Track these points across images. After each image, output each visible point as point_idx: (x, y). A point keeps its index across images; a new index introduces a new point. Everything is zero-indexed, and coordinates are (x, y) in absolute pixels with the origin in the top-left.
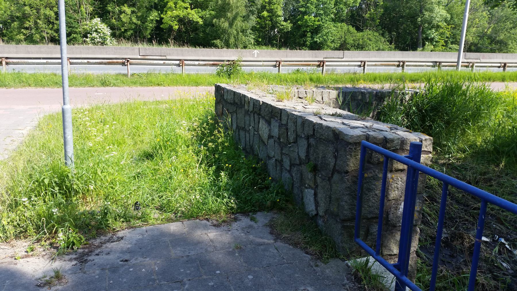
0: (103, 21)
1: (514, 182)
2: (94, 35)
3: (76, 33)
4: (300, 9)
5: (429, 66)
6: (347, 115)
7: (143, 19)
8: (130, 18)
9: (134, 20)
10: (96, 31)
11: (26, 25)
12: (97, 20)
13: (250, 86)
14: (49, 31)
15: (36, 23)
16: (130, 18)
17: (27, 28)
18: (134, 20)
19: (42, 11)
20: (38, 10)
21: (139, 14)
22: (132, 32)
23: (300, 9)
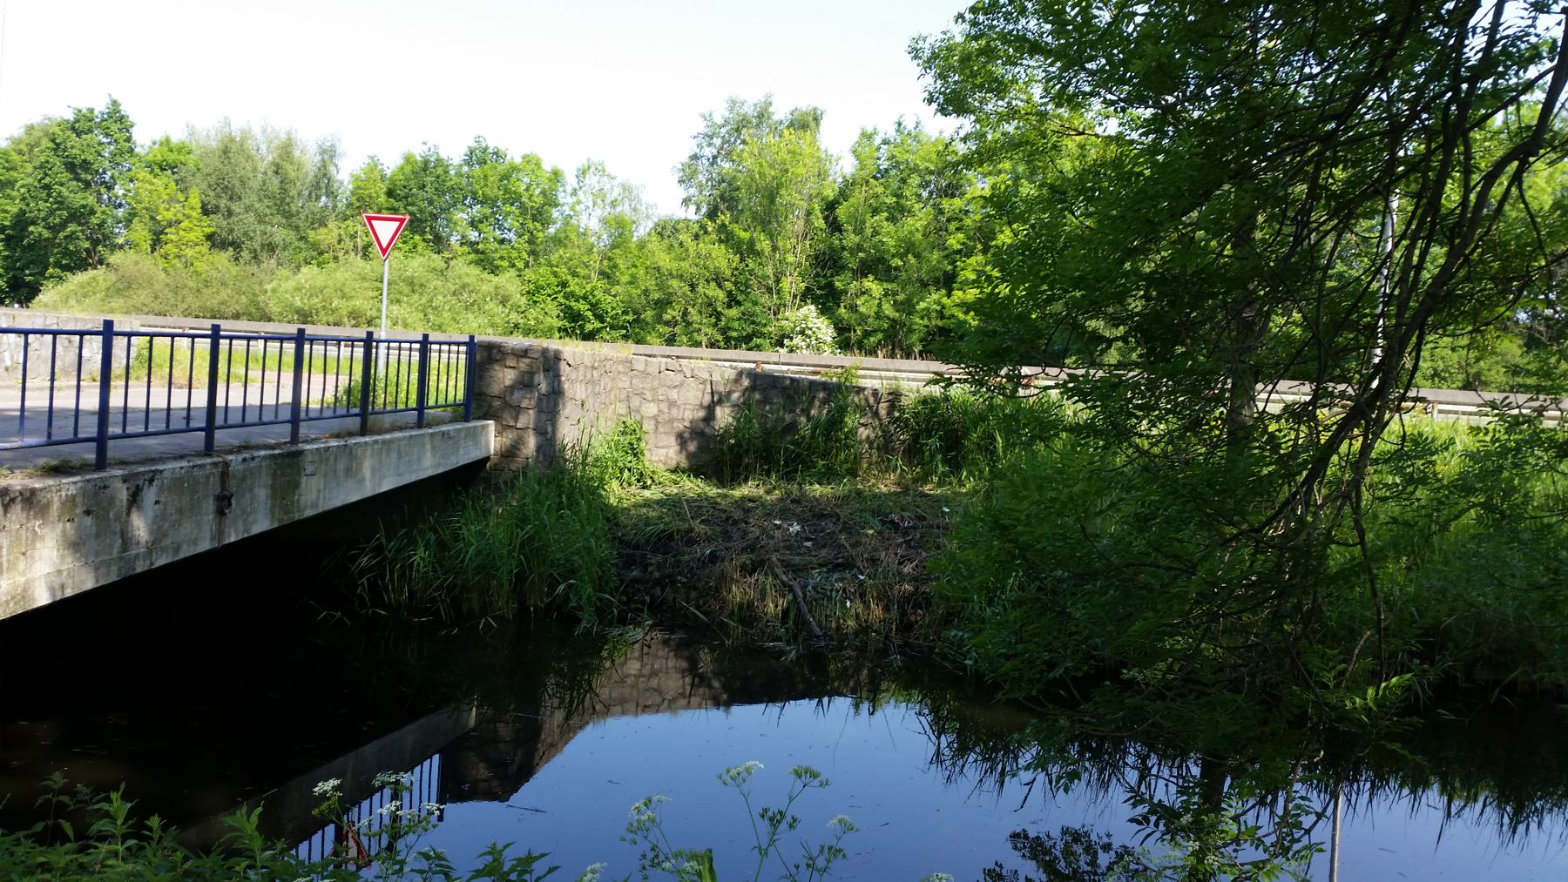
0: (824, 311)
1: (1564, 366)
2: (798, 340)
3: (762, 335)
4: (1516, 163)
5: (1470, 414)
6: (702, 497)
7: (907, 307)
8: (880, 305)
9: (888, 310)
10: (802, 333)
11: (666, 317)
12: (810, 309)
13: (90, 486)
14: (709, 331)
15: (685, 313)
16: (880, 305)
17: (667, 323)
18: (888, 310)
19: (700, 289)
20: (693, 287)
21: (901, 297)
22: (880, 336)
23: (1516, 163)
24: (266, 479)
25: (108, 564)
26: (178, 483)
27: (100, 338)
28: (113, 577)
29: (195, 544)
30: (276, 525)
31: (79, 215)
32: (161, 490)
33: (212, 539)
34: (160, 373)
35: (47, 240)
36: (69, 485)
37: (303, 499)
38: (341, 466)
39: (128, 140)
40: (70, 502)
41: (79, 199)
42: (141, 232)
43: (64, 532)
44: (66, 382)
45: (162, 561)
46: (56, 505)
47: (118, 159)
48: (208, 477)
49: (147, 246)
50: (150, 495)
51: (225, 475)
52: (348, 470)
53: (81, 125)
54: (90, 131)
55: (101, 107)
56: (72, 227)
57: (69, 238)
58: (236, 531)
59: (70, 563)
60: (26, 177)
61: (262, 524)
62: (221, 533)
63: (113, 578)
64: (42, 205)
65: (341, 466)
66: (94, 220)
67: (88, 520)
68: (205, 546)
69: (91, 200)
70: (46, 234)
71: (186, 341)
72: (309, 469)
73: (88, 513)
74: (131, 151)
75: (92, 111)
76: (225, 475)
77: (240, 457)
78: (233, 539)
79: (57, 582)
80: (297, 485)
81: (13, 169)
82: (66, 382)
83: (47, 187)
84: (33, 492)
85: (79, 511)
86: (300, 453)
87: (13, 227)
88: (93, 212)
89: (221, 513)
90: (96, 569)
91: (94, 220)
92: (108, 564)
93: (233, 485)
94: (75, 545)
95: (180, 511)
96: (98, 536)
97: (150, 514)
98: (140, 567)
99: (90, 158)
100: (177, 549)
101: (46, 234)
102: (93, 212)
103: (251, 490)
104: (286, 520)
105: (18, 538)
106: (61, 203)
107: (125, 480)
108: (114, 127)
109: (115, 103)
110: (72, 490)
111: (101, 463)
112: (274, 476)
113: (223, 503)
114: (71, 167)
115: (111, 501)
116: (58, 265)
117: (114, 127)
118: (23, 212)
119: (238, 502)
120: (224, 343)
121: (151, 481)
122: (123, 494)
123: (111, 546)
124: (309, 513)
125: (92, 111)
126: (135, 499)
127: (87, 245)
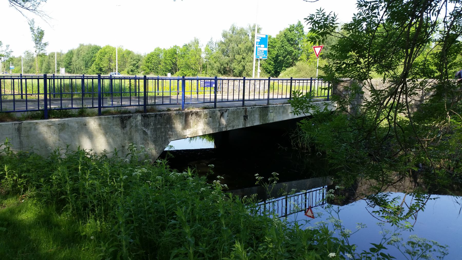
24: (258, 112)
25: (216, 128)
26: (233, 112)
27: (43, 80)
28: (217, 131)
29: (238, 126)
30: (261, 124)
31: (290, 53)
32: (229, 114)
33: (243, 125)
34: (276, 91)
35: (283, 60)
36: (206, 111)
37: (269, 118)
38: (281, 111)
39: (302, 31)
40: (206, 115)
41: (290, 48)
42: (304, 56)
43: (205, 121)
44: (252, 93)
45: (229, 129)
46: (203, 115)
47: (300, 37)
48: (241, 111)
49: (305, 60)
50: (226, 114)
51: (246, 111)
52: (283, 112)
53: (290, 30)
54: (293, 30)
55: (296, 23)
56: (288, 56)
57: (287, 59)
58: (250, 124)
59: (206, 127)
60: (278, 45)
61: (257, 123)
62: (245, 124)
63: (217, 131)
64: (282, 51)
65: (281, 111)
66: (293, 54)
67: (211, 119)
68: (241, 127)
69: (293, 49)
70: (282, 59)
71: (195, 81)
72: (271, 111)
73: (210, 117)
74: (303, 34)
75: (294, 25)
76: (246, 111)
77: (250, 107)
78: (249, 126)
79: (204, 131)
80: (267, 115)
81: (276, 43)
82: (252, 93)
83: (283, 46)
84: (197, 112)
85: (208, 116)
86: (269, 107)
87: (276, 58)
88: (293, 52)
89: (245, 120)
90: (213, 129)
91: (293, 54)
92: (216, 128)
93: (248, 114)
94: (208, 124)
95: (234, 118)
96: (213, 122)
97: (226, 119)
98: (224, 130)
99: (293, 38)
100: (233, 127)
101: (282, 59)
102: (293, 52)
103: (254, 115)
104: (264, 123)
105: (194, 121)
106: (286, 50)
107: (219, 111)
108: (299, 28)
109: (299, 22)
110: (207, 112)
111: (215, 107)
112: (260, 112)
113: (246, 117)
114: (288, 41)
115: (216, 115)
116: (285, 66)
117: (299, 28)
118: (278, 54)
119: (250, 118)
120: (48, 80)
121: (226, 111)
122: (219, 114)
123: (216, 125)
124: (271, 122)
125: (294, 25)
126: (222, 115)
127: (291, 61)
